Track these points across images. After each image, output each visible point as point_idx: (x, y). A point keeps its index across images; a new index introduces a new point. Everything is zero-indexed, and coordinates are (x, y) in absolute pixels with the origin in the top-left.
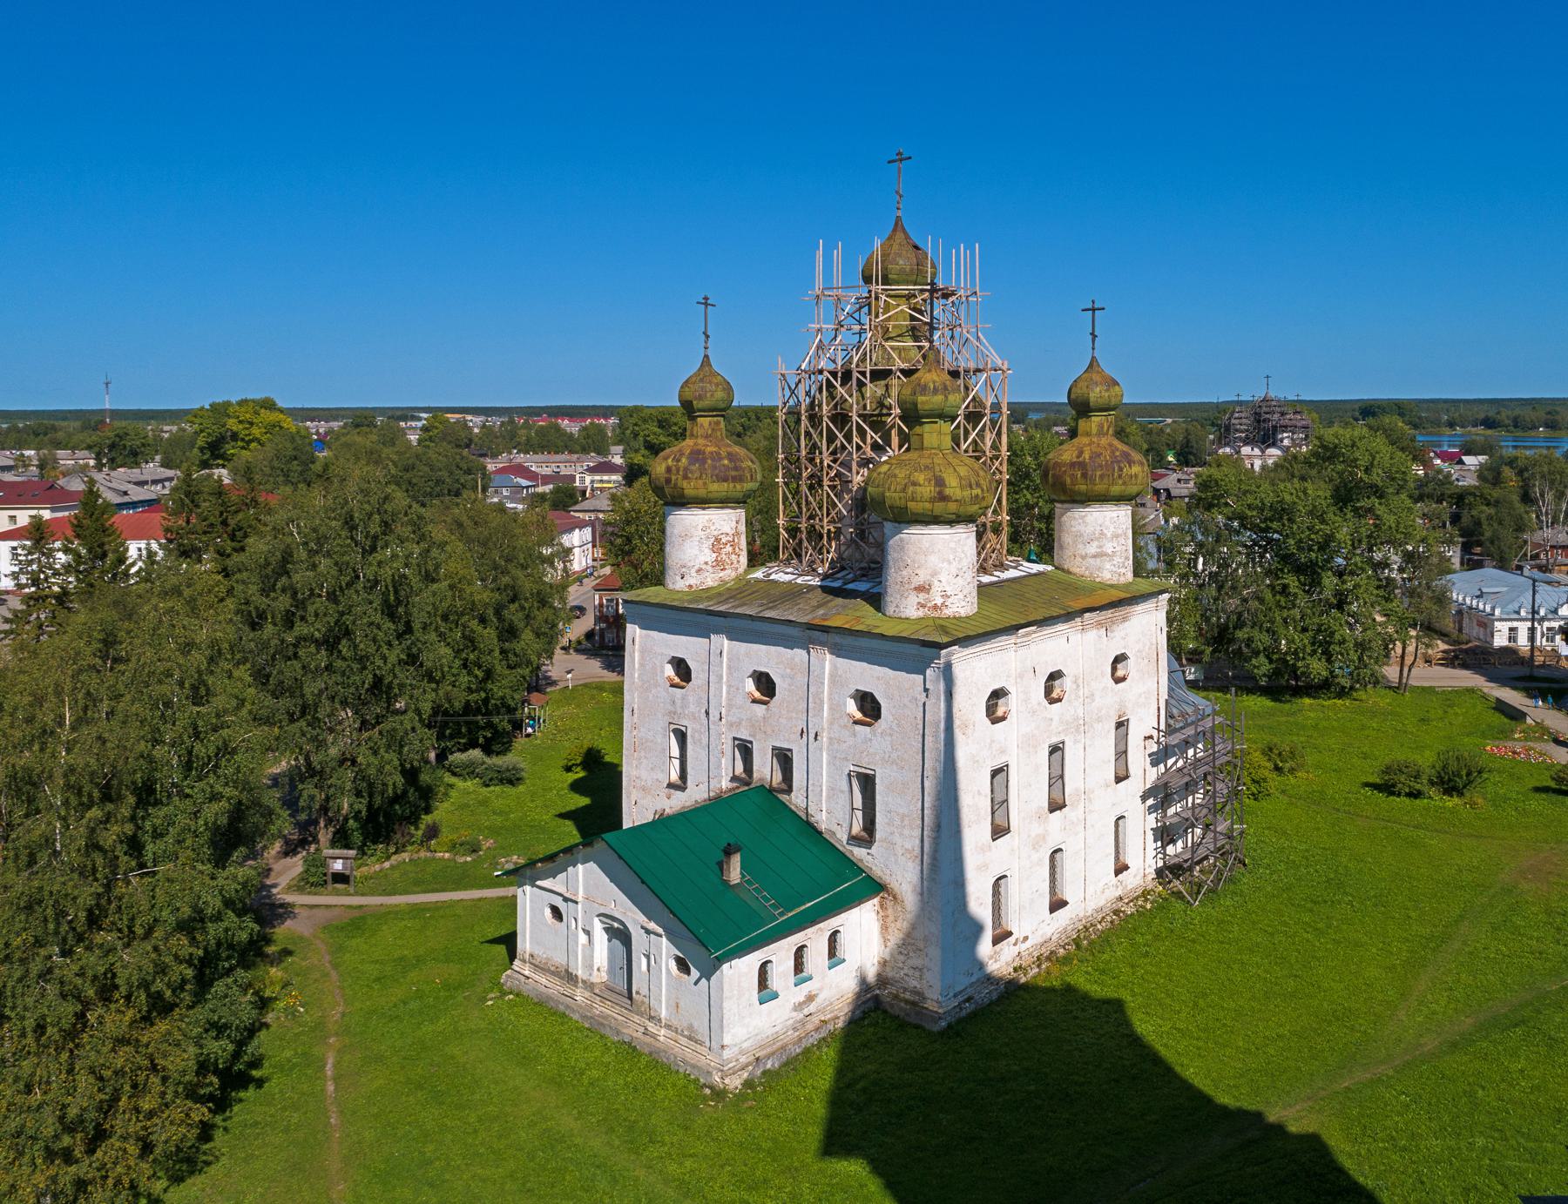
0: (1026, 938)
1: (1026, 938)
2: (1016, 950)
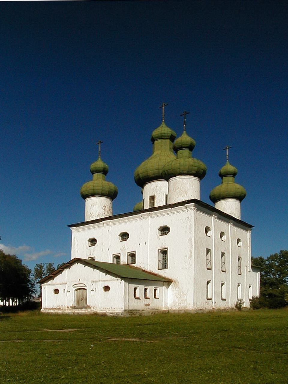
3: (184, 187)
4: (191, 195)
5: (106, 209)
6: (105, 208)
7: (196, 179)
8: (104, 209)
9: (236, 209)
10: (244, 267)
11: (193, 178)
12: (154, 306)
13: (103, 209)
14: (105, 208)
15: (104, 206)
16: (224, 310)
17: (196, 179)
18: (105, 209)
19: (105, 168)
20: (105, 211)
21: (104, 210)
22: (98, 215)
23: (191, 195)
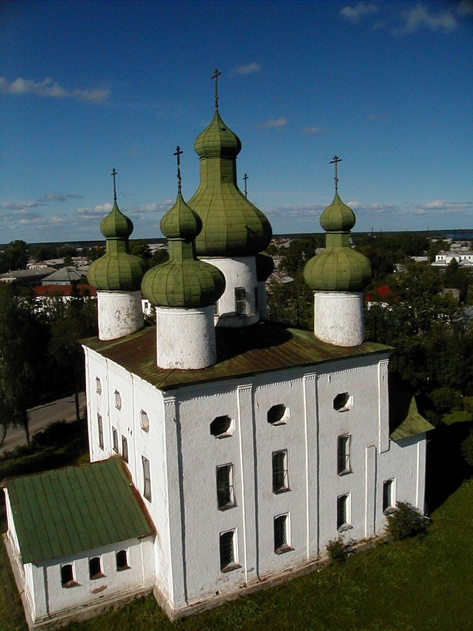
3: (169, 333)
4: (182, 352)
5: (121, 317)
6: (120, 314)
7: (191, 313)
8: (117, 317)
9: (345, 316)
10: (365, 449)
11: (184, 313)
12: (116, 586)
13: (115, 316)
14: (120, 314)
15: (117, 311)
16: (387, 489)
17: (191, 313)
18: (118, 316)
19: (120, 230)
20: (119, 319)
21: (117, 320)
22: (109, 329)
23: (182, 352)
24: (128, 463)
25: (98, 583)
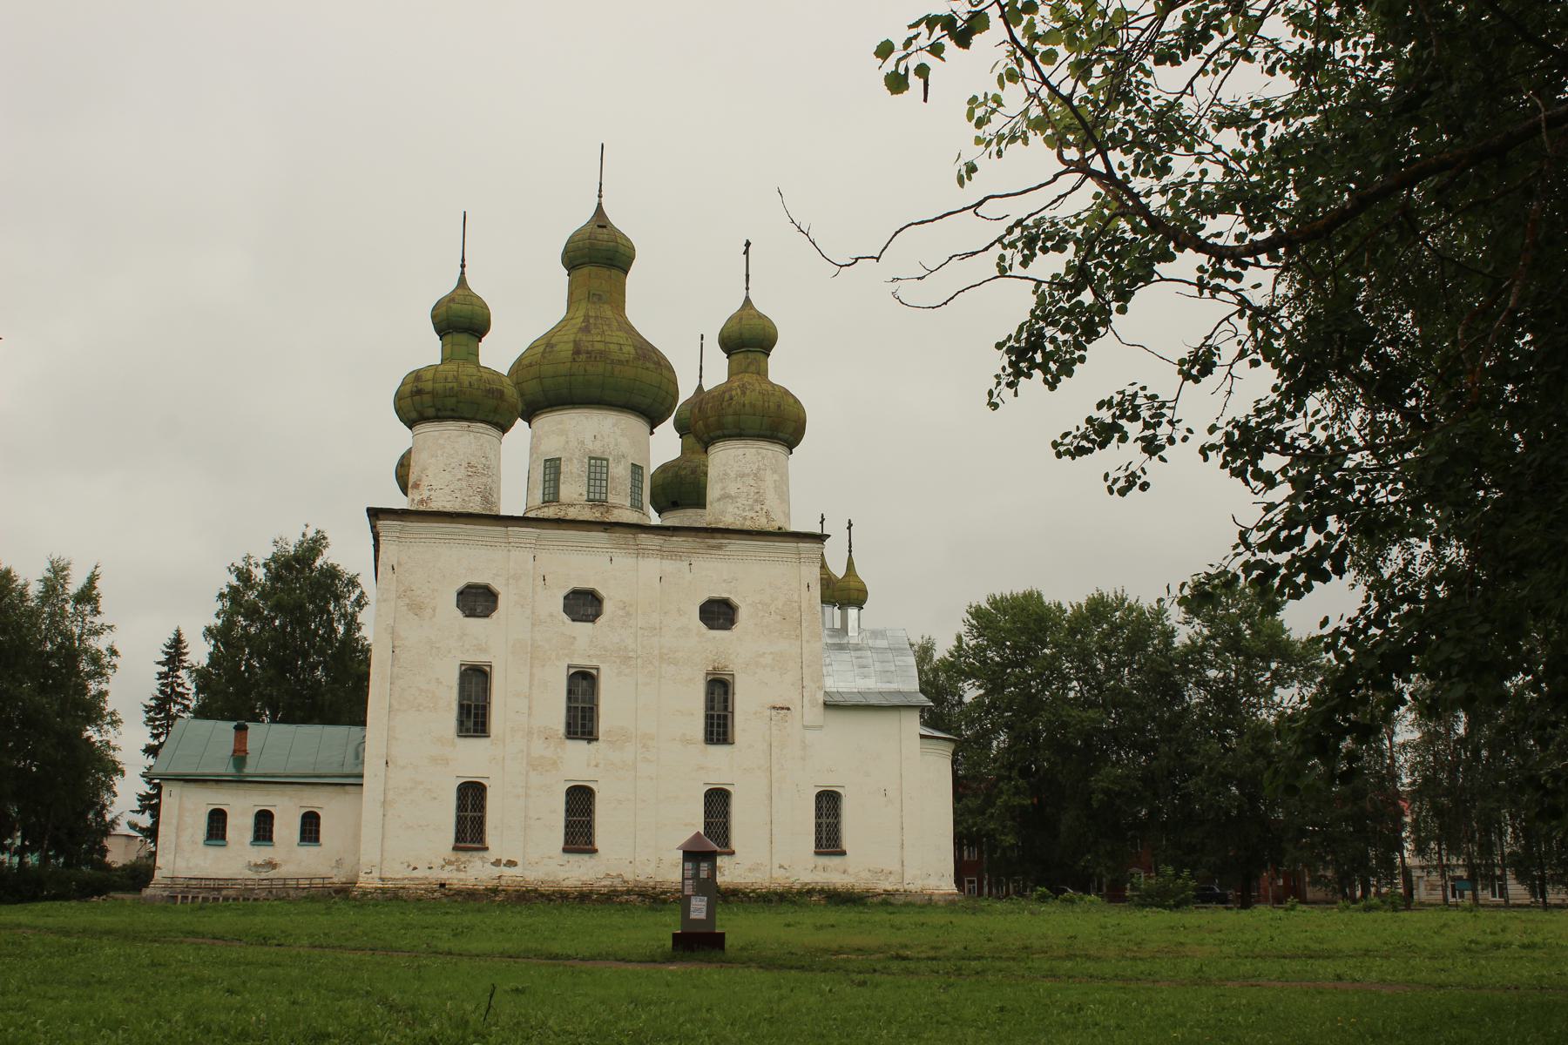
0: (511, 864)
1: (511, 864)
2: (496, 871)
24: (1122, 310)
25: (262, 854)
